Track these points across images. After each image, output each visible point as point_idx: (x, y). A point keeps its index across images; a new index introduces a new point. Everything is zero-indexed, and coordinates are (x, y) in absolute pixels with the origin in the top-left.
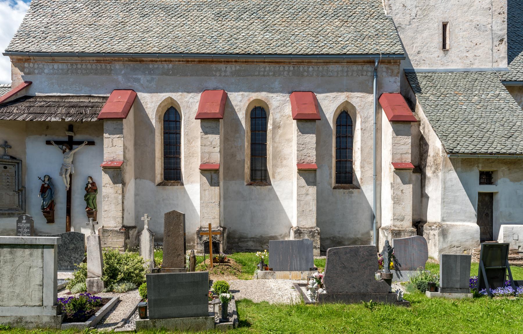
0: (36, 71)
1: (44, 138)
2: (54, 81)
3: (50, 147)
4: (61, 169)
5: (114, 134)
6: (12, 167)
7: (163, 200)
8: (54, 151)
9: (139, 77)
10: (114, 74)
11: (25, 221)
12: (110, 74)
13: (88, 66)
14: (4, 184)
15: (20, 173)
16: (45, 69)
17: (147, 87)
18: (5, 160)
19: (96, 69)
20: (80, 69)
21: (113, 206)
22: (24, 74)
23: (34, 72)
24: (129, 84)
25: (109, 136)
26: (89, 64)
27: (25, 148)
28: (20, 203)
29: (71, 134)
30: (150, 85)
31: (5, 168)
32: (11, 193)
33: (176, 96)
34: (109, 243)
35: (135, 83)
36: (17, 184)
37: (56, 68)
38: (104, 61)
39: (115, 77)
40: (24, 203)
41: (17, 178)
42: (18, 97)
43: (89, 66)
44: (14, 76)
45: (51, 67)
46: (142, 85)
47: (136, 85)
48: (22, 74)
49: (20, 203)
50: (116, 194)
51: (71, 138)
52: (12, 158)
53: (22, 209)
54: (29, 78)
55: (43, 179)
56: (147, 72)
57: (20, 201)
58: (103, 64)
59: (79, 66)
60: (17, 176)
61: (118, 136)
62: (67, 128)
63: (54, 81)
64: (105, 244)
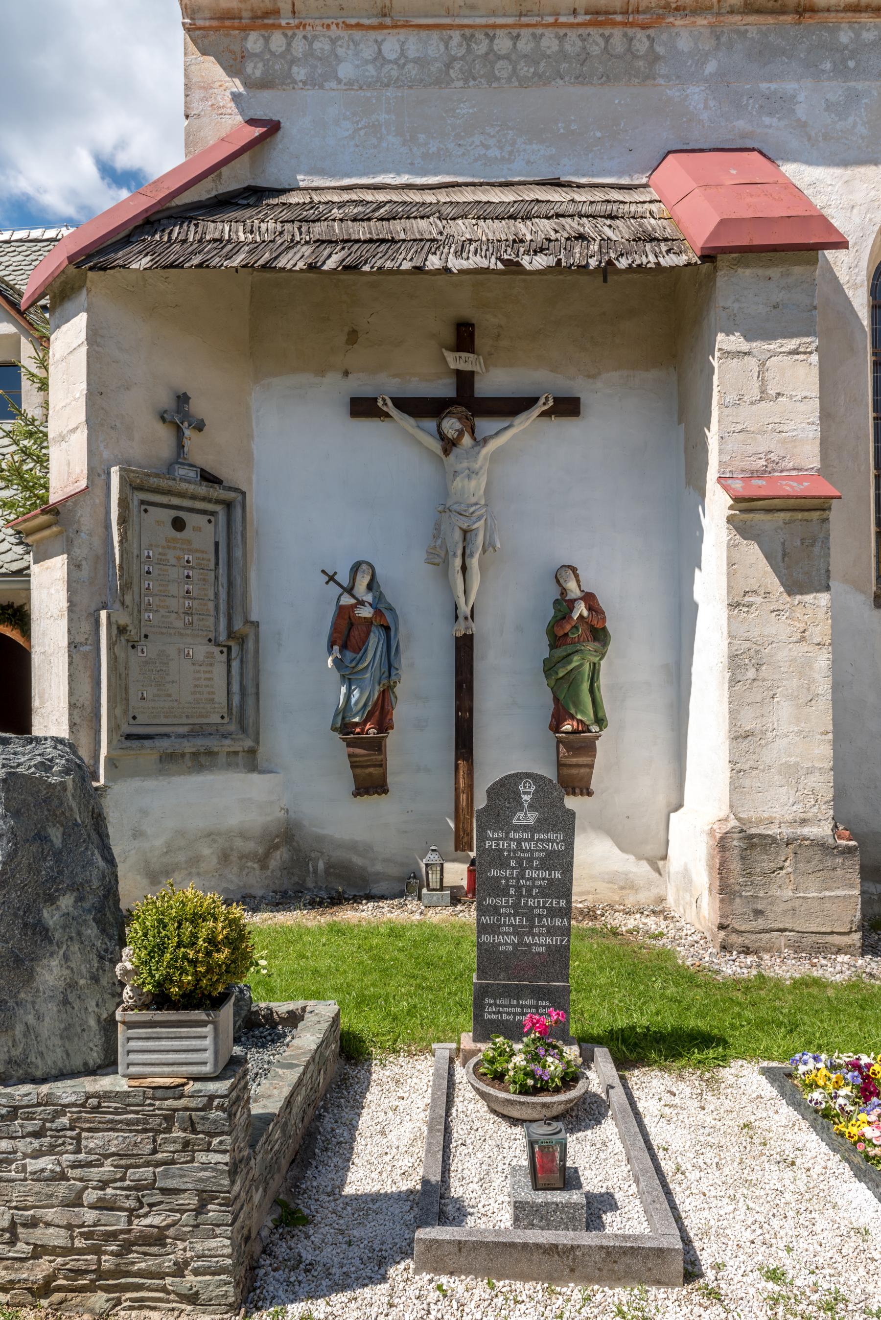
0: (300, 73)
1: (336, 389)
2: (383, 117)
3: (368, 427)
4: (437, 532)
6: (201, 520)
8: (396, 451)
9: (790, 86)
10: (667, 77)
12: (649, 77)
13: (544, 42)
14: (173, 603)
15: (238, 553)
16: (339, 60)
19: (585, 57)
20: (506, 57)
22: (245, 84)
23: (289, 75)
25: (745, 346)
26: (549, 33)
27: (250, 437)
28: (236, 700)
29: (457, 361)
31: (178, 524)
32: (201, 650)
34: (780, 908)
35: (767, 120)
36: (223, 606)
37: (392, 56)
38: (625, 13)
39: (673, 93)
40: (250, 701)
41: (223, 579)
43: (549, 42)
44: (197, 94)
45: (368, 52)
46: (804, 125)
47: (772, 128)
48: (237, 85)
49: (236, 700)
50: (803, 647)
51: (465, 379)
52: (208, 478)
53: (243, 729)
54: (268, 105)
55: (344, 578)
56: (828, 66)
57: (236, 687)
58: (617, 32)
59: (503, 44)
60: (222, 570)
61: (792, 344)
63: (383, 117)
64: (758, 913)
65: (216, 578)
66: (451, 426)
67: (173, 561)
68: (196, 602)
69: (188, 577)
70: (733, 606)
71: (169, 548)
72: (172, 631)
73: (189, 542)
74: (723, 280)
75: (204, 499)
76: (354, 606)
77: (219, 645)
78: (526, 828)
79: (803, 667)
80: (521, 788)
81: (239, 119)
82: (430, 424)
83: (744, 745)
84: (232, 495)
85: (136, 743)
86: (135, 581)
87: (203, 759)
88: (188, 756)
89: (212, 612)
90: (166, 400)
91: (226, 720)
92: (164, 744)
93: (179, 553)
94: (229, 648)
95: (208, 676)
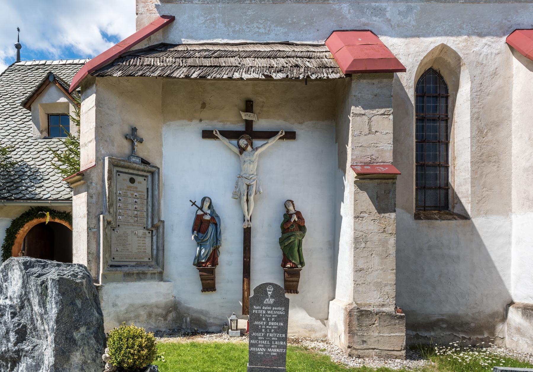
3: (209, 142)
5: (372, 108)
6: (141, 179)
7: (430, 248)
9: (384, 5)
11: (272, 301)
14: (130, 213)
15: (156, 193)
17: (398, 26)
18: (135, 165)
21: (376, 260)
24: (363, 20)
25: (363, 112)
27: (162, 145)
29: (245, 116)
30: (404, 21)
31: (132, 181)
33: (454, 43)
34: (372, 340)
35: (374, 18)
36: (150, 214)
39: (336, 7)
40: (161, 253)
41: (150, 203)
42: (151, 44)
47: (376, 22)
49: (155, 252)
50: (384, 235)
51: (249, 124)
52: (144, 162)
53: (158, 264)
54: (170, 9)
55: (199, 204)
57: (155, 247)
61: (382, 111)
62: (242, 105)
63: (217, 15)
64: (364, 342)
65: (147, 203)
66: (243, 142)
67: (130, 195)
68: (139, 212)
69: (136, 202)
70: (356, 217)
71: (128, 190)
72: (129, 224)
73: (136, 188)
74: (354, 84)
75: (142, 171)
76: (202, 215)
77: (148, 230)
78: (269, 305)
79: (383, 243)
80: (268, 289)
81: (158, 15)
82: (235, 142)
83: (359, 274)
84: (154, 169)
85: (114, 269)
86: (114, 203)
87: (141, 276)
88: (135, 274)
89: (145, 217)
90: (127, 130)
91: (151, 260)
92: (126, 269)
93: (132, 192)
94: (152, 231)
95: (143, 242)
